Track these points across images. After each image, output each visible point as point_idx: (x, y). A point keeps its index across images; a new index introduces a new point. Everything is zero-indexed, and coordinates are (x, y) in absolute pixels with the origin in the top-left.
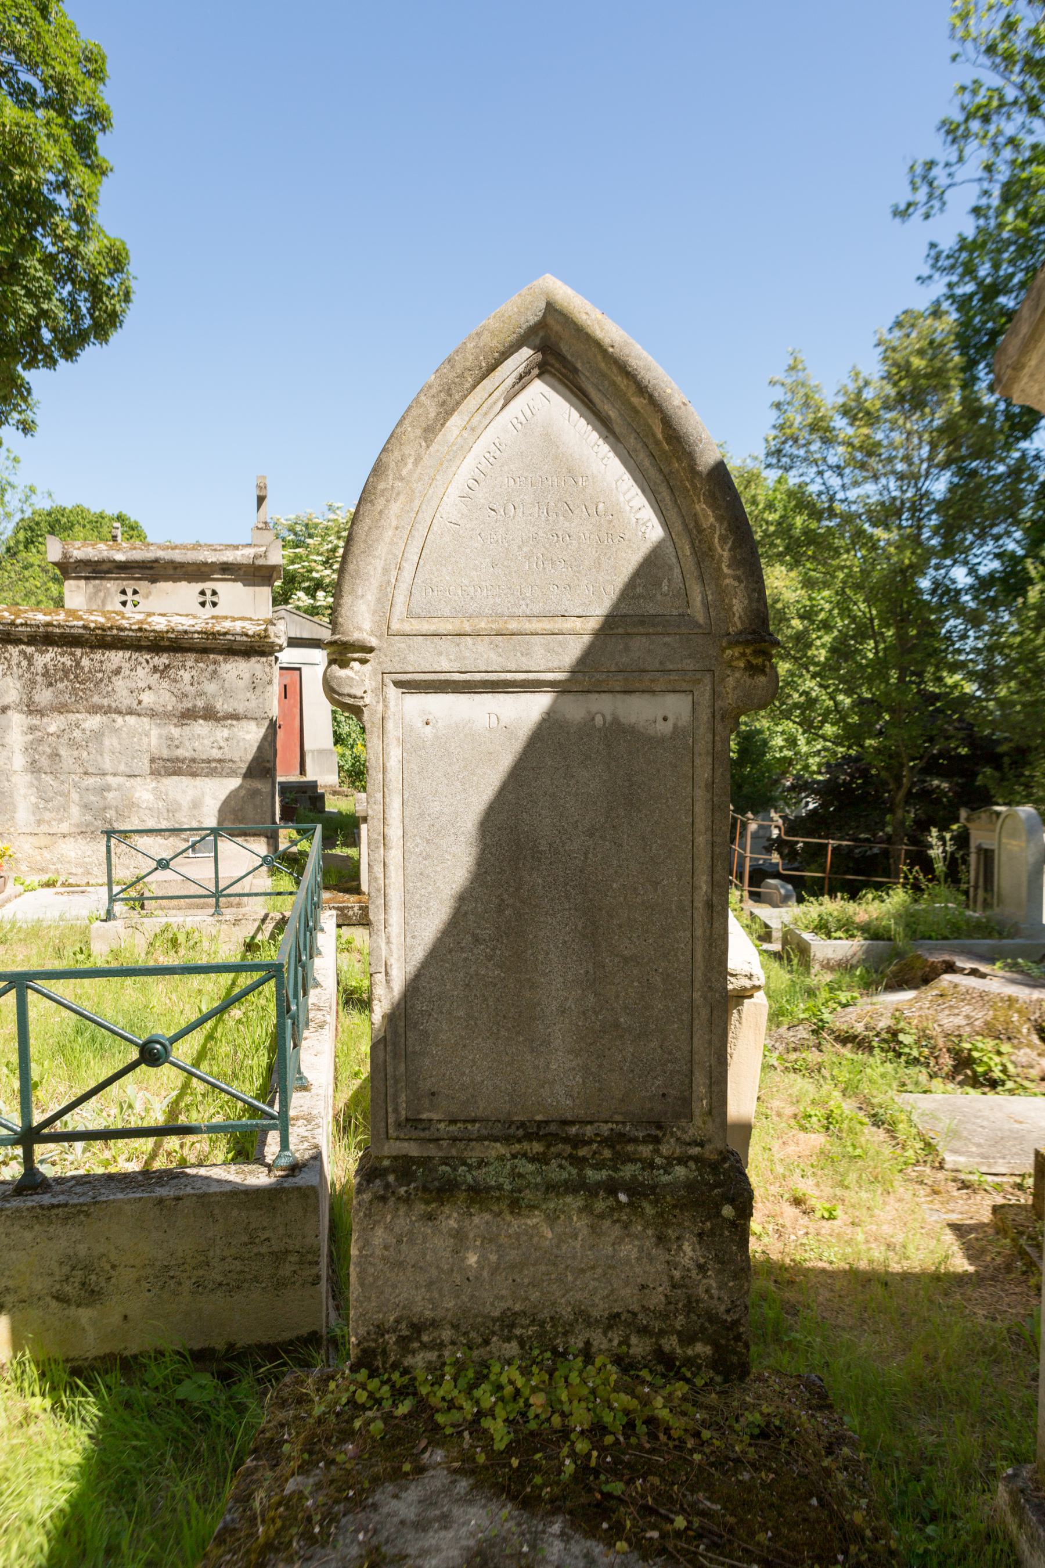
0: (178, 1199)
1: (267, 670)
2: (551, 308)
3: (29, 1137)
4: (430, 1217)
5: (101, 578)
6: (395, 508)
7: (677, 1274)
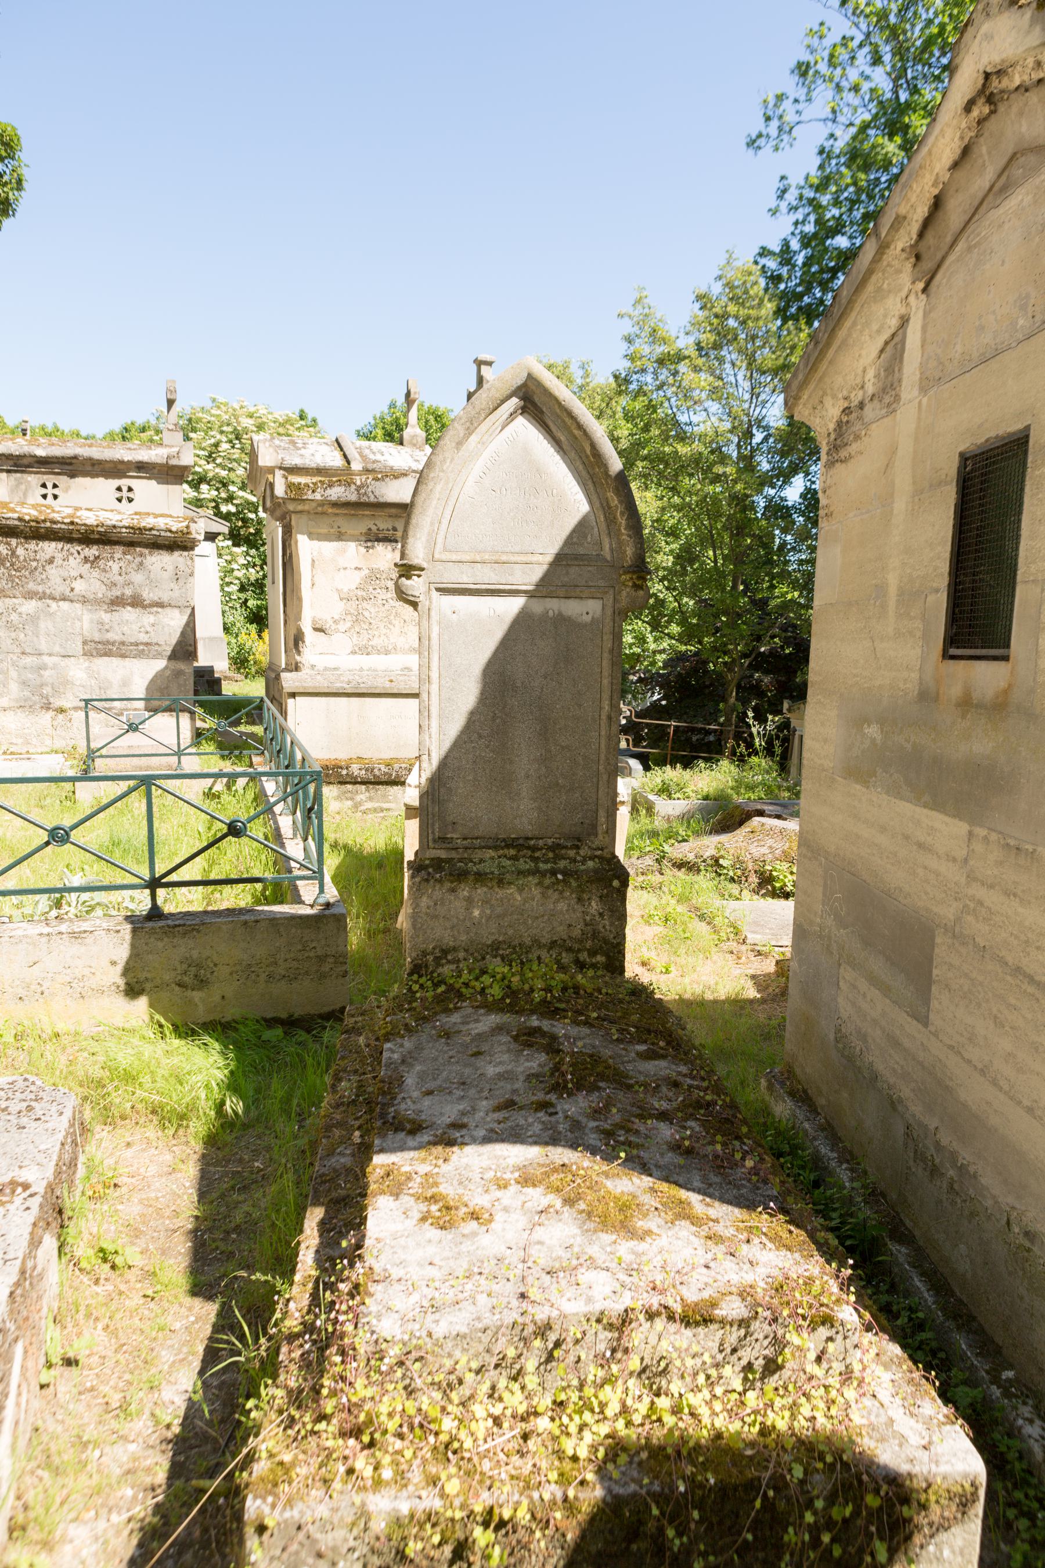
0: (257, 921)
1: (189, 563)
2: (530, 376)
3: (154, 884)
4: (453, 890)
5: (22, 472)
6: (439, 488)
7: (588, 918)
